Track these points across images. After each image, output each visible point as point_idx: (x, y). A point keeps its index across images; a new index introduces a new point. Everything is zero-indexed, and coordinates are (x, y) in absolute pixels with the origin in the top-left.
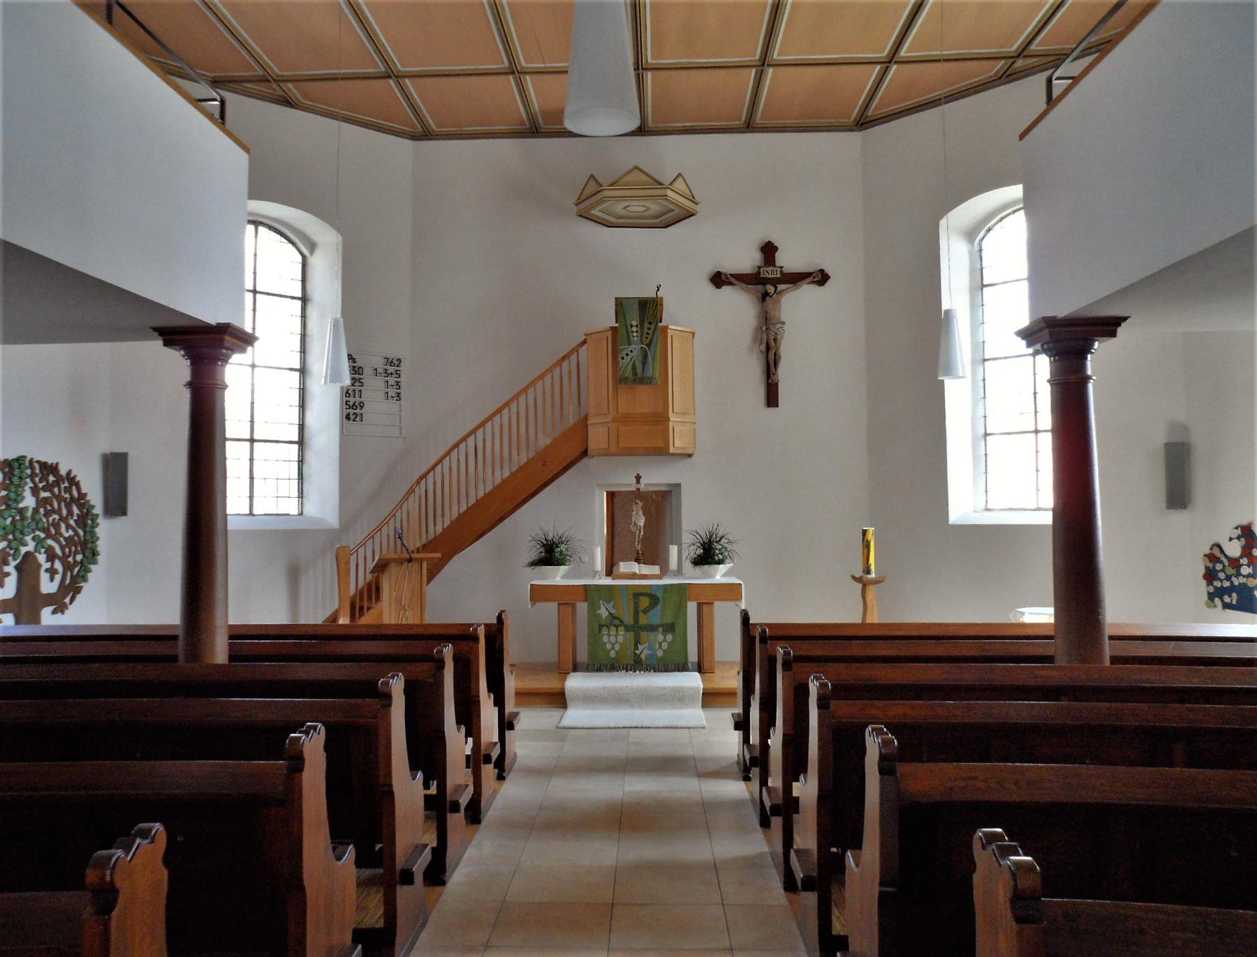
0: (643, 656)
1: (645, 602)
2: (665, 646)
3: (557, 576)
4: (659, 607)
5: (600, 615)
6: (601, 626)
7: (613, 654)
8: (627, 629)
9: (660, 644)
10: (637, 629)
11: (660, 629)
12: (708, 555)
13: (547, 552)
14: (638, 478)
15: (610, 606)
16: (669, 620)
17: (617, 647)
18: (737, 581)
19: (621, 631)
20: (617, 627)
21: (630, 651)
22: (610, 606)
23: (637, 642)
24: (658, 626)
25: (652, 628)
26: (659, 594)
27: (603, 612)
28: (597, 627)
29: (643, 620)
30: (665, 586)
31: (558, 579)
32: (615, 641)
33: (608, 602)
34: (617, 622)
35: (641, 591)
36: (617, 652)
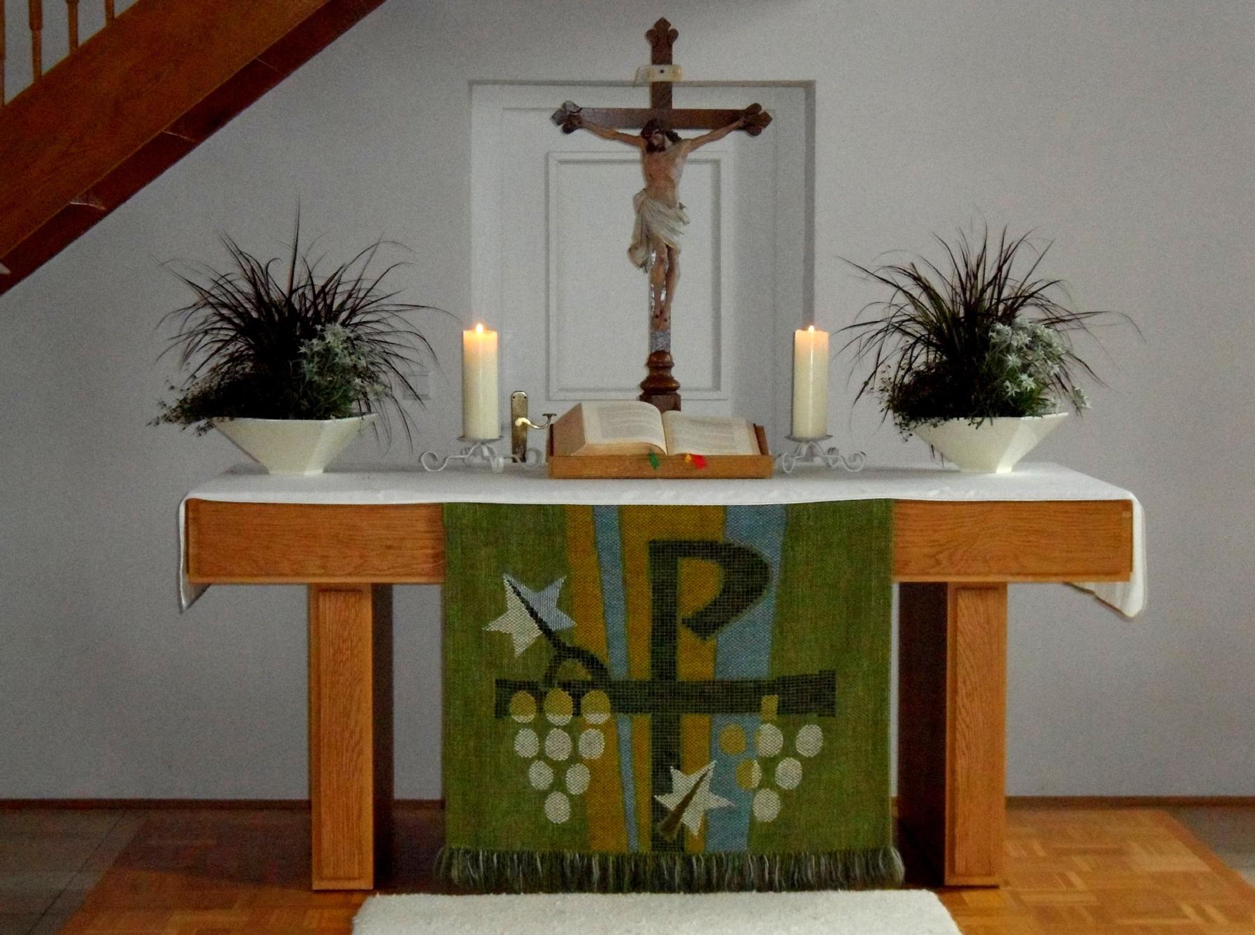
0: (692, 820)
1: (700, 583)
2: (789, 773)
3: (298, 465)
4: (762, 610)
5: (504, 639)
6: (507, 687)
7: (558, 810)
8: (624, 699)
9: (769, 765)
10: (667, 705)
11: (770, 703)
12: (964, 362)
13: (259, 357)
14: (662, 40)
15: (548, 601)
16: (807, 663)
17: (577, 780)
18: (1130, 496)
19: (598, 713)
20: (577, 693)
21: (636, 795)
22: (548, 601)
23: (666, 758)
24: (761, 688)
25: (736, 698)
26: (769, 549)
27: (515, 626)
28: (489, 694)
29: (694, 662)
30: (793, 515)
31: (313, 472)
32: (568, 756)
33: (539, 585)
34: (581, 673)
35: (690, 532)
36: (578, 803)
